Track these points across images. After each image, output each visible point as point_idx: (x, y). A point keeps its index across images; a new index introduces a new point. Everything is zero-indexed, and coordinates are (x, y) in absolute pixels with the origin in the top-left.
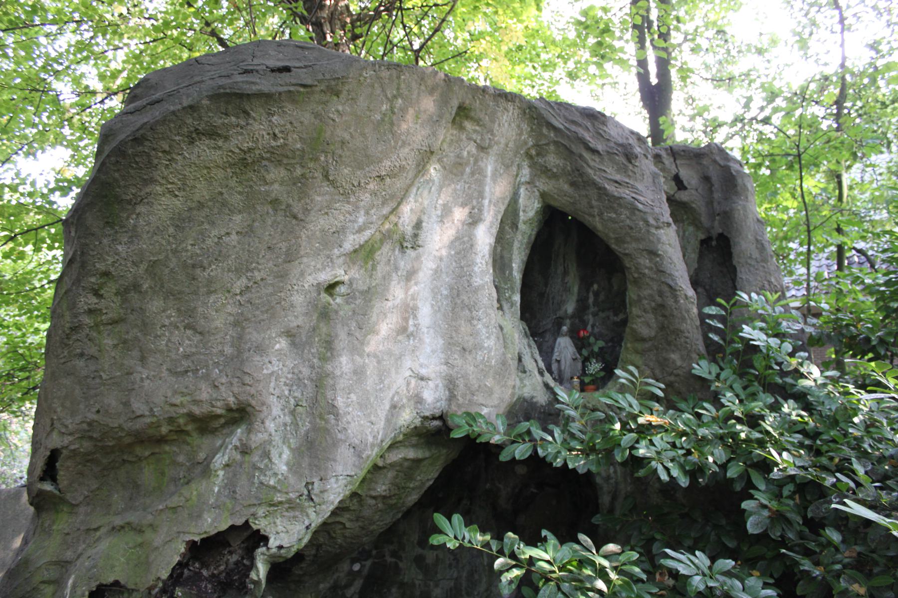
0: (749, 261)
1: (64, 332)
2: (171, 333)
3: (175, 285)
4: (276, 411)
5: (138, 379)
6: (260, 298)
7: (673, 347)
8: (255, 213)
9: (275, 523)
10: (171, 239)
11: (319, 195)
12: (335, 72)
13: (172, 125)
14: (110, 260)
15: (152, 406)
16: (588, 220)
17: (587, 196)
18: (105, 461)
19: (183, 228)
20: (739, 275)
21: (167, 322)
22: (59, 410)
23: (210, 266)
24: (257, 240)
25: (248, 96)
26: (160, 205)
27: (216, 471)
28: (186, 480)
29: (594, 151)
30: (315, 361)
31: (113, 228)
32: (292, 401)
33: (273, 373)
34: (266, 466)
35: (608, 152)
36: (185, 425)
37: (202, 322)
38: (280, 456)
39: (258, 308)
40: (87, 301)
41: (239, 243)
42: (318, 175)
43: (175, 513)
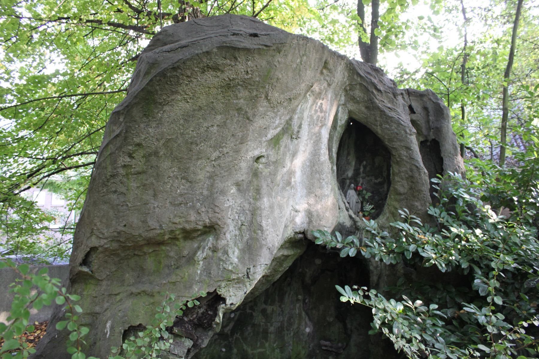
0: (450, 155)
1: (106, 177)
2: (173, 181)
3: (179, 153)
4: (231, 228)
5: (152, 207)
6: (225, 163)
7: (416, 199)
8: (229, 115)
9: (229, 291)
10: (181, 127)
11: (261, 107)
12: (281, 39)
13: (195, 62)
14: (143, 137)
15: (162, 223)
16: (374, 128)
17: (374, 115)
18: (123, 255)
19: (189, 121)
20: (444, 162)
21: (172, 175)
22: (98, 224)
23: (201, 143)
24: (227, 130)
25: (239, 49)
26: (178, 106)
27: (199, 262)
28: (176, 266)
29: (379, 91)
30: (251, 200)
31: (148, 118)
32: (240, 223)
33: (230, 206)
34: (226, 259)
35: (385, 91)
36: (179, 235)
37: (192, 175)
38: (233, 254)
39: (223, 169)
40: (124, 160)
41: (217, 131)
42: (263, 96)
43: (175, 285)
